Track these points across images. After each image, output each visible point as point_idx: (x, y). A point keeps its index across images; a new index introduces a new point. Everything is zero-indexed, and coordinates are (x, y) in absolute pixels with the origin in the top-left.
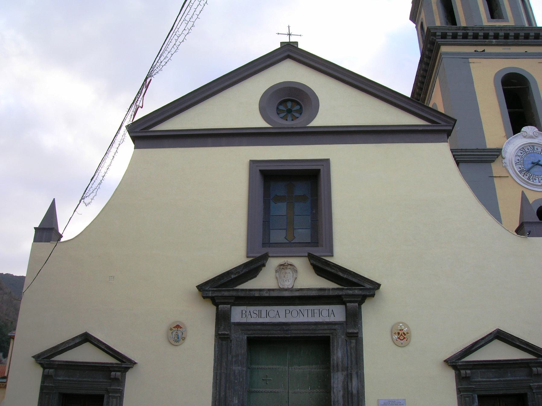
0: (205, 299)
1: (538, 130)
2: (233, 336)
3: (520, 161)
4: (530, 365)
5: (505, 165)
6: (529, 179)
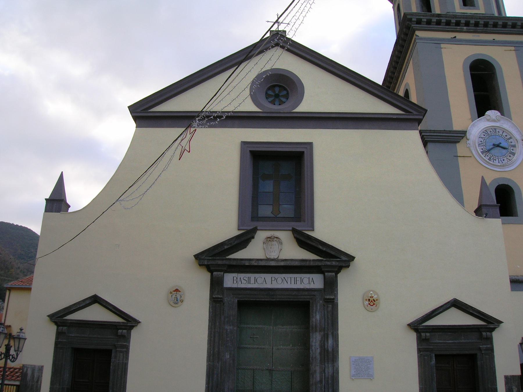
0: (201, 266)
1: (500, 114)
2: (226, 299)
3: (482, 143)
4: (481, 330)
6: (490, 159)
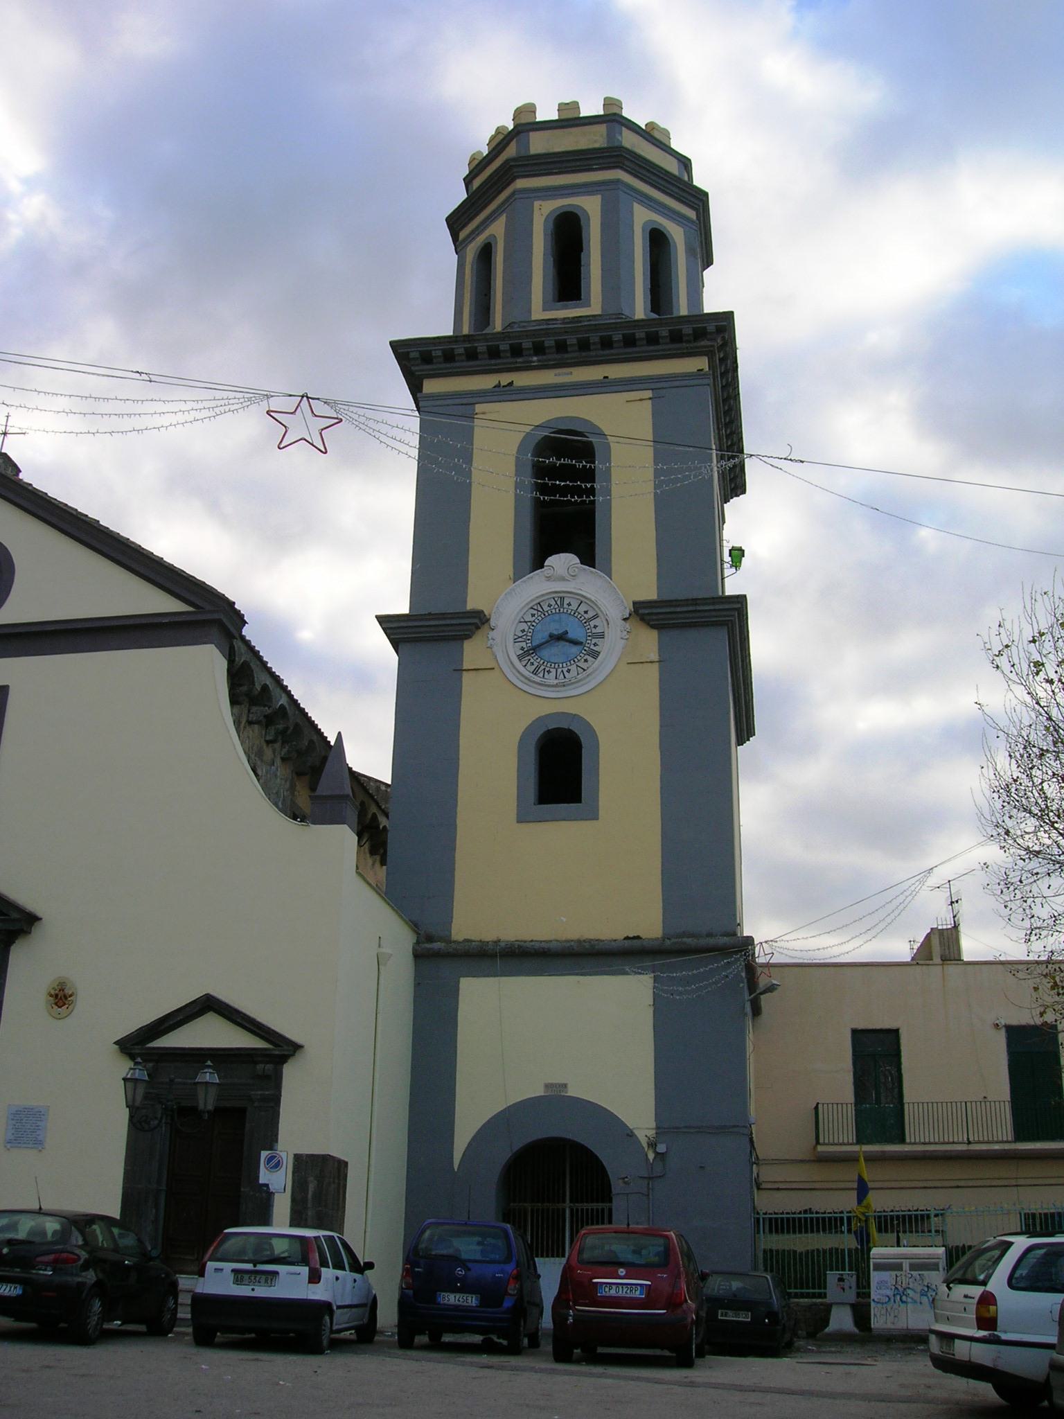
3: (525, 633)
5: (491, 645)
6: (535, 672)
